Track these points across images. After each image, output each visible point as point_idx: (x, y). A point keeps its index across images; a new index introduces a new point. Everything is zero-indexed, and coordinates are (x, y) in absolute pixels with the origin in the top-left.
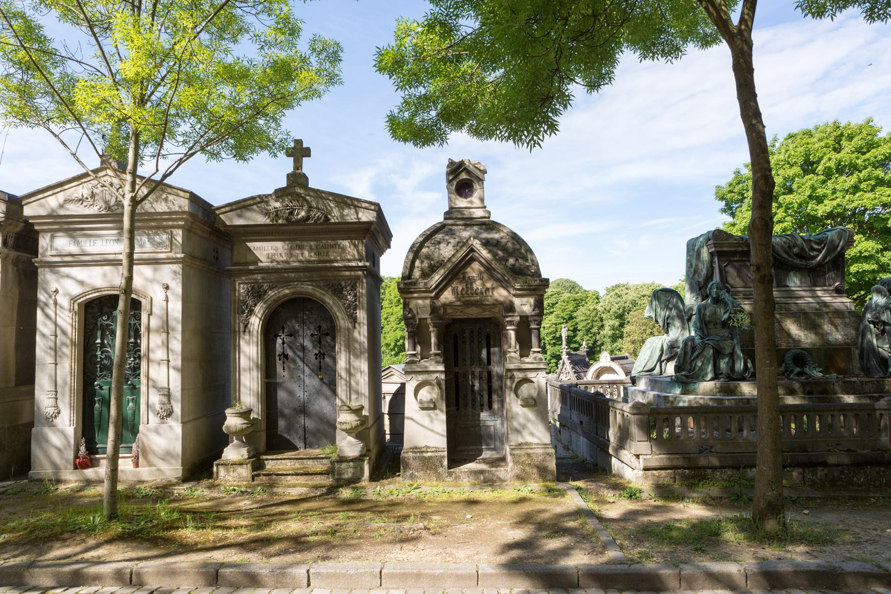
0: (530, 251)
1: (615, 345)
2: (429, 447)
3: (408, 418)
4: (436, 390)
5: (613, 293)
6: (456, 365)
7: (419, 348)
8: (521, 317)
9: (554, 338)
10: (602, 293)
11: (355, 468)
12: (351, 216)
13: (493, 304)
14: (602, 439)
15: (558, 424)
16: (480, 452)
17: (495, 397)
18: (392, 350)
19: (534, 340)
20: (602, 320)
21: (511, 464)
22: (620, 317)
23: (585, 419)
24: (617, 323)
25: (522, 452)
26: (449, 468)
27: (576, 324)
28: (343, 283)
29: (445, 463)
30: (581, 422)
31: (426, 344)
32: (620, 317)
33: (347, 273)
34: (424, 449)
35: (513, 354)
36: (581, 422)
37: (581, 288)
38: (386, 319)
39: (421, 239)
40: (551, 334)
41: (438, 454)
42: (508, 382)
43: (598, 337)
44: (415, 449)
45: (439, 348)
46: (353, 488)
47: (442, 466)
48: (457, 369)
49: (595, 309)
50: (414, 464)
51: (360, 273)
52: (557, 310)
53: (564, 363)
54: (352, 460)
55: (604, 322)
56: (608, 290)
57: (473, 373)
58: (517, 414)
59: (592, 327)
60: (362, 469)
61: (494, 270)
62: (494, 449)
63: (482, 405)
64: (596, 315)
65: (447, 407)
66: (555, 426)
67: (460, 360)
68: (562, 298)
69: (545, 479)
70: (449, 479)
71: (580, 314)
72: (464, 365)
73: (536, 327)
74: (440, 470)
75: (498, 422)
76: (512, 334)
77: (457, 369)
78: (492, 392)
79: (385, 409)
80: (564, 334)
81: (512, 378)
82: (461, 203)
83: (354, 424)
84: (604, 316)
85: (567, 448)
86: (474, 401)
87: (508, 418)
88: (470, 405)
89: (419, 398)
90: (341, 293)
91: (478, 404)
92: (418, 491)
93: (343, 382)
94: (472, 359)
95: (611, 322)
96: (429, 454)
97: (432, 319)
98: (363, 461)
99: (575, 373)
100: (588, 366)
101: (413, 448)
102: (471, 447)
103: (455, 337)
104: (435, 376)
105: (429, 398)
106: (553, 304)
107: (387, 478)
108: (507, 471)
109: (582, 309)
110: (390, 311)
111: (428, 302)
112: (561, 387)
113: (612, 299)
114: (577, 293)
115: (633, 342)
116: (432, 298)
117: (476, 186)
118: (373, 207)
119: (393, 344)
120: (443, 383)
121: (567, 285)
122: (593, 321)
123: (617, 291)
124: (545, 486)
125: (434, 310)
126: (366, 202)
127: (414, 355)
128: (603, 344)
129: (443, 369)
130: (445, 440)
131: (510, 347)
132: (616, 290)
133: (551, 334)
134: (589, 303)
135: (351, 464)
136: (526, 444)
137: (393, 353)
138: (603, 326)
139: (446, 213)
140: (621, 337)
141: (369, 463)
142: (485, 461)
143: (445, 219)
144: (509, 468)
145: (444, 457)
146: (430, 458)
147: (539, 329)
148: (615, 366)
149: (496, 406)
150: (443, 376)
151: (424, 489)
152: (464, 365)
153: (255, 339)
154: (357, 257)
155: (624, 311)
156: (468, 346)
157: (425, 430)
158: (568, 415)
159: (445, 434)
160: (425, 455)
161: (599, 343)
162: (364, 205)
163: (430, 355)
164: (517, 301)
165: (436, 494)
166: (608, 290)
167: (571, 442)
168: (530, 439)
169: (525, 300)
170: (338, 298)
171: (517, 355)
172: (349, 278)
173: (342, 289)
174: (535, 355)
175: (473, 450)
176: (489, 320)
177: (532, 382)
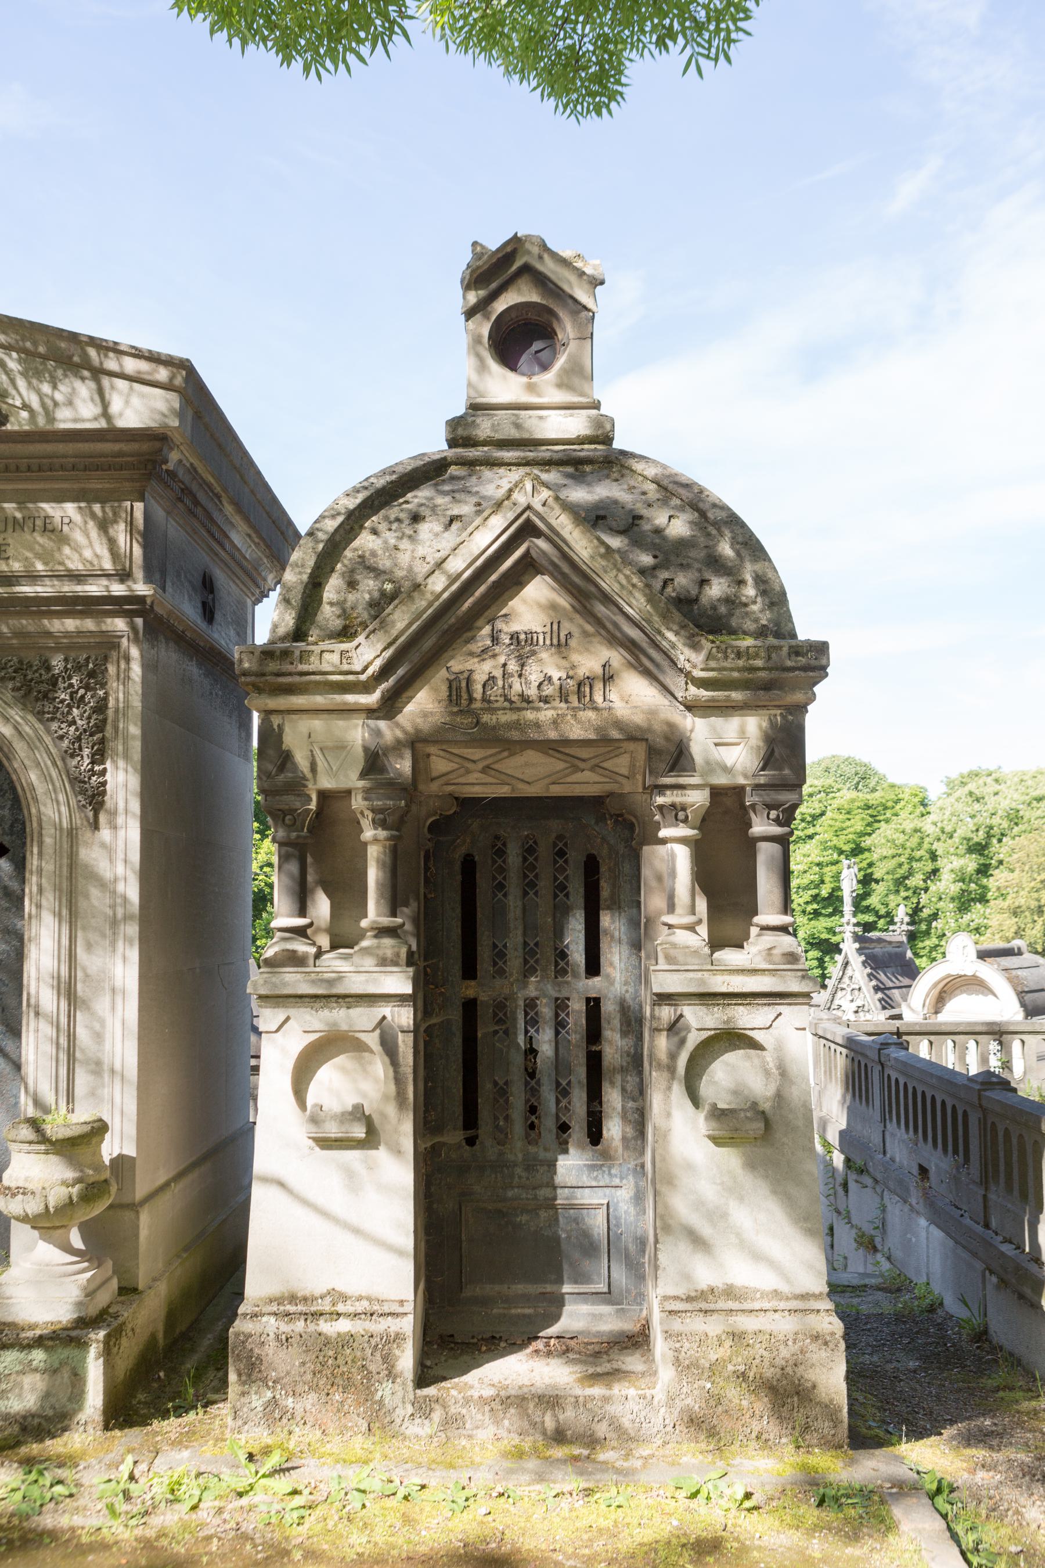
0: (751, 547)
1: (967, 917)
2: (344, 1298)
3: (266, 1180)
4: (379, 1067)
5: (962, 792)
6: (469, 971)
7: (322, 906)
8: (716, 793)
9: (815, 898)
10: (935, 792)
11: (52, 1371)
12: (77, 407)
13: (603, 740)
14: (1007, 1249)
15: (838, 1160)
16: (554, 1307)
17: (613, 1098)
19: (766, 885)
20: (934, 856)
21: (666, 1374)
22: (979, 849)
23: (939, 1162)
24: (971, 863)
25: (713, 1327)
26: (424, 1378)
27: (871, 865)
28: (57, 663)
29: (406, 1360)
30: (923, 1171)
31: (347, 893)
32: (979, 849)
33: (71, 624)
34: (326, 1306)
35: (683, 937)
36: (923, 1171)
37: (882, 778)
39: (352, 503)
40: (806, 888)
41: (379, 1326)
42: (662, 1043)
43: (924, 898)
44: (295, 1304)
45: (394, 903)
46: (28, 1463)
47: (392, 1375)
48: (470, 990)
49: (916, 831)
50: (281, 1361)
51: (120, 624)
52: (823, 828)
53: (846, 964)
54: (39, 1342)
55: (940, 863)
56: (950, 784)
57: (531, 1004)
58: (690, 1167)
59: (910, 873)
60: (78, 1378)
61: (607, 599)
62: (608, 1296)
63: (564, 1128)
64: (920, 845)
65: (418, 1134)
66: (829, 1165)
67: (484, 953)
68: (836, 804)
69: (802, 1434)
70: (420, 1429)
71: (882, 843)
72: (501, 973)
73: (777, 830)
74: (385, 1391)
75: (623, 1197)
76: (682, 858)
77: (470, 990)
78: (597, 1076)
79: (392, 681)
80: (849, 887)
81: (675, 1027)
82: (504, 386)
83: (57, 1196)
84: (939, 848)
85: (869, 1244)
86: (533, 1110)
87: (655, 1182)
88: (518, 1128)
89: (311, 1100)
90: (46, 696)
91: (549, 1124)
92: (282, 1484)
93: (47, 1030)
94: (530, 952)
95: (957, 863)
96: (343, 1326)
97: (367, 793)
98: (82, 1345)
99: (877, 989)
100: (912, 972)
101: (279, 1300)
102: (520, 1288)
103: (469, 866)
105: (350, 1101)
106: (814, 818)
107: (180, 1411)
108: (649, 1397)
109: (885, 830)
112: (850, 1044)
113: (959, 806)
114: (874, 790)
115: (1016, 912)
116: (371, 712)
117: (567, 329)
118: (162, 374)
120: (405, 1045)
121: (850, 771)
122: (911, 859)
123: (971, 787)
124: (804, 1468)
126: (138, 354)
127: (300, 932)
128: (935, 916)
130: (406, 1269)
131: (671, 908)
132: (969, 786)
133: (806, 888)
134: (903, 814)
135: (38, 1356)
136: (730, 1292)
138: (935, 871)
139: (454, 424)
140: (983, 899)
141: (108, 1352)
142: (567, 1348)
143: (452, 443)
144: (659, 1393)
145: (399, 1338)
146: (347, 1341)
147: (784, 842)
148: (988, 972)
149: (614, 1129)
150: (404, 1017)
151: (311, 1472)
152: (501, 973)
154: (108, 565)
155: (989, 836)
156: (514, 903)
157: (334, 1219)
158: (876, 1139)
159: (406, 1240)
160: (327, 1327)
161: (926, 913)
162: (131, 365)
163: (362, 936)
164: (701, 734)
165: (355, 1501)
166: (950, 784)
167: (883, 1226)
168: (741, 1272)
169: (730, 726)
170: (39, 715)
171: (698, 940)
172: (70, 644)
173: (54, 682)
174: (770, 939)
175: (526, 1299)
176: (595, 804)
177: (755, 1045)
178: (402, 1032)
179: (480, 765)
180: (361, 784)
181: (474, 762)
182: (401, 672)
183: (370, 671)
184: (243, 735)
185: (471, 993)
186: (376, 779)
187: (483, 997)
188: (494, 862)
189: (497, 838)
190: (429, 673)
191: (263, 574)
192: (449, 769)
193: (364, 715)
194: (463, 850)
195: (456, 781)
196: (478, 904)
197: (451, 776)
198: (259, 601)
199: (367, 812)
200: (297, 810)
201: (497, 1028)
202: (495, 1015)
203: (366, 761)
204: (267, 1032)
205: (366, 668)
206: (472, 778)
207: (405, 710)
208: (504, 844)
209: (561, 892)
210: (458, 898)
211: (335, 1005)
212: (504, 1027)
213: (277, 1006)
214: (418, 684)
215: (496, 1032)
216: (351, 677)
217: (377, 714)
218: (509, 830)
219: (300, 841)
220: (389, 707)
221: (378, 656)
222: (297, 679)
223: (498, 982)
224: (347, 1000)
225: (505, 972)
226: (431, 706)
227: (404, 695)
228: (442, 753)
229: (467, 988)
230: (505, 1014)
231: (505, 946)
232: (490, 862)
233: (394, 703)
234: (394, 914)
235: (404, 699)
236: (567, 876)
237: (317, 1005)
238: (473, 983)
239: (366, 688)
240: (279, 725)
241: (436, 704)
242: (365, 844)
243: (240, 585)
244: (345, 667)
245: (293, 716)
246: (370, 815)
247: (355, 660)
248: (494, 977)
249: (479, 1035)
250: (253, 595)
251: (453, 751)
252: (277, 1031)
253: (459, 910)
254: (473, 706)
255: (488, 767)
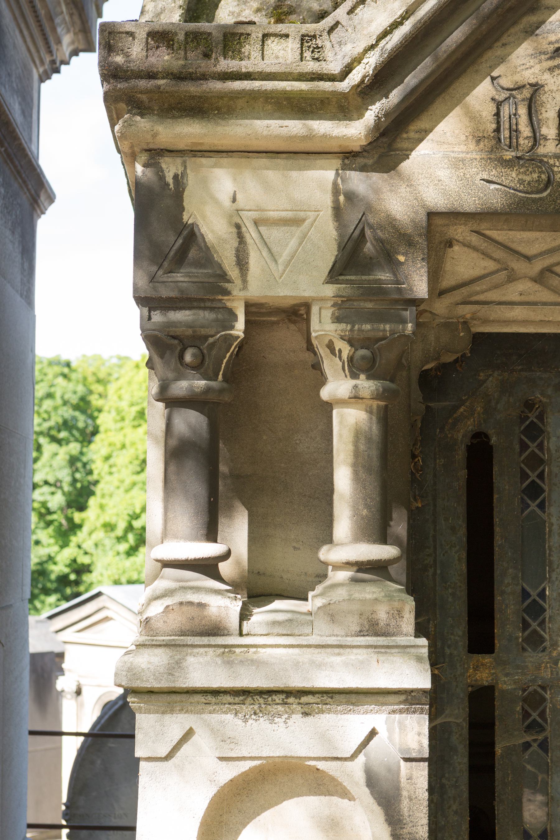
6: (481, 640)
7: (237, 533)
18: (119, 539)
38: (107, 458)
79: (395, 96)
97: (344, 312)
103: (480, 454)
104: (350, 726)
110: (117, 439)
111: (317, 184)
116: (349, 157)
119: (122, 526)
125: (361, 254)
129: (420, 679)
137: (123, 547)
150: (413, 732)
153: (347, 544)
178: (407, 760)
179: (538, 266)
180: (330, 290)
181: (528, 258)
182: (411, 80)
183: (355, 77)
184: (26, 265)
185: (484, 677)
186: (362, 282)
187: (506, 684)
188: (524, 447)
189: (529, 405)
190: (458, 87)
191: (59, 30)
192: (477, 272)
193: (337, 162)
194: (470, 425)
195: (481, 297)
196: (496, 520)
197: (477, 287)
198: (45, 77)
199: (340, 345)
200: (206, 337)
201: (528, 739)
202: (526, 715)
203: (342, 248)
204: (149, 759)
205: (347, 70)
206: (513, 292)
207: (414, 154)
208: (541, 417)
209: (534, 499)
210: (462, 510)
211: (280, 708)
212: (540, 738)
213: (170, 709)
214: (438, 106)
215: (527, 746)
216: (327, 86)
217: (361, 161)
218: (549, 391)
219: (211, 397)
220: (386, 149)
221: (372, 47)
222: (218, 86)
223: (531, 657)
224: (304, 699)
225: (542, 640)
226: (463, 148)
227: (413, 127)
228: (474, 239)
229: (476, 668)
230: (542, 714)
231: (542, 594)
232: (517, 447)
233: (394, 140)
234: (211, 534)
235: (412, 135)
236: (522, 480)
237: (247, 709)
238: (487, 659)
239: (343, 108)
240: (176, 177)
241: (472, 146)
242: (327, 408)
243: (28, 40)
244: (310, 66)
245: (204, 161)
246: (346, 350)
247: (328, 53)
248: (524, 649)
249: (498, 751)
250: (42, 63)
251: (494, 234)
252: (168, 758)
253: (462, 531)
254: (541, 150)
255: (549, 269)
